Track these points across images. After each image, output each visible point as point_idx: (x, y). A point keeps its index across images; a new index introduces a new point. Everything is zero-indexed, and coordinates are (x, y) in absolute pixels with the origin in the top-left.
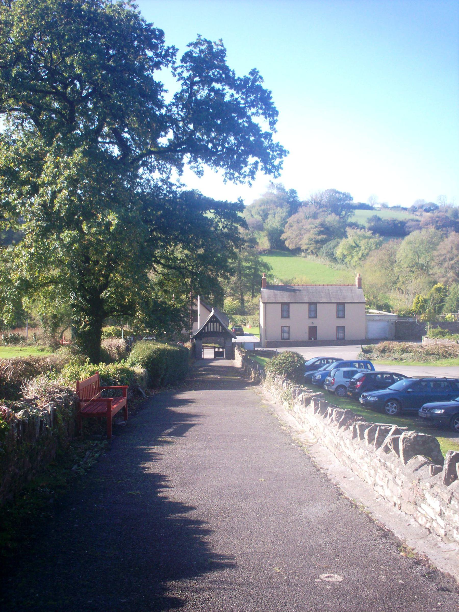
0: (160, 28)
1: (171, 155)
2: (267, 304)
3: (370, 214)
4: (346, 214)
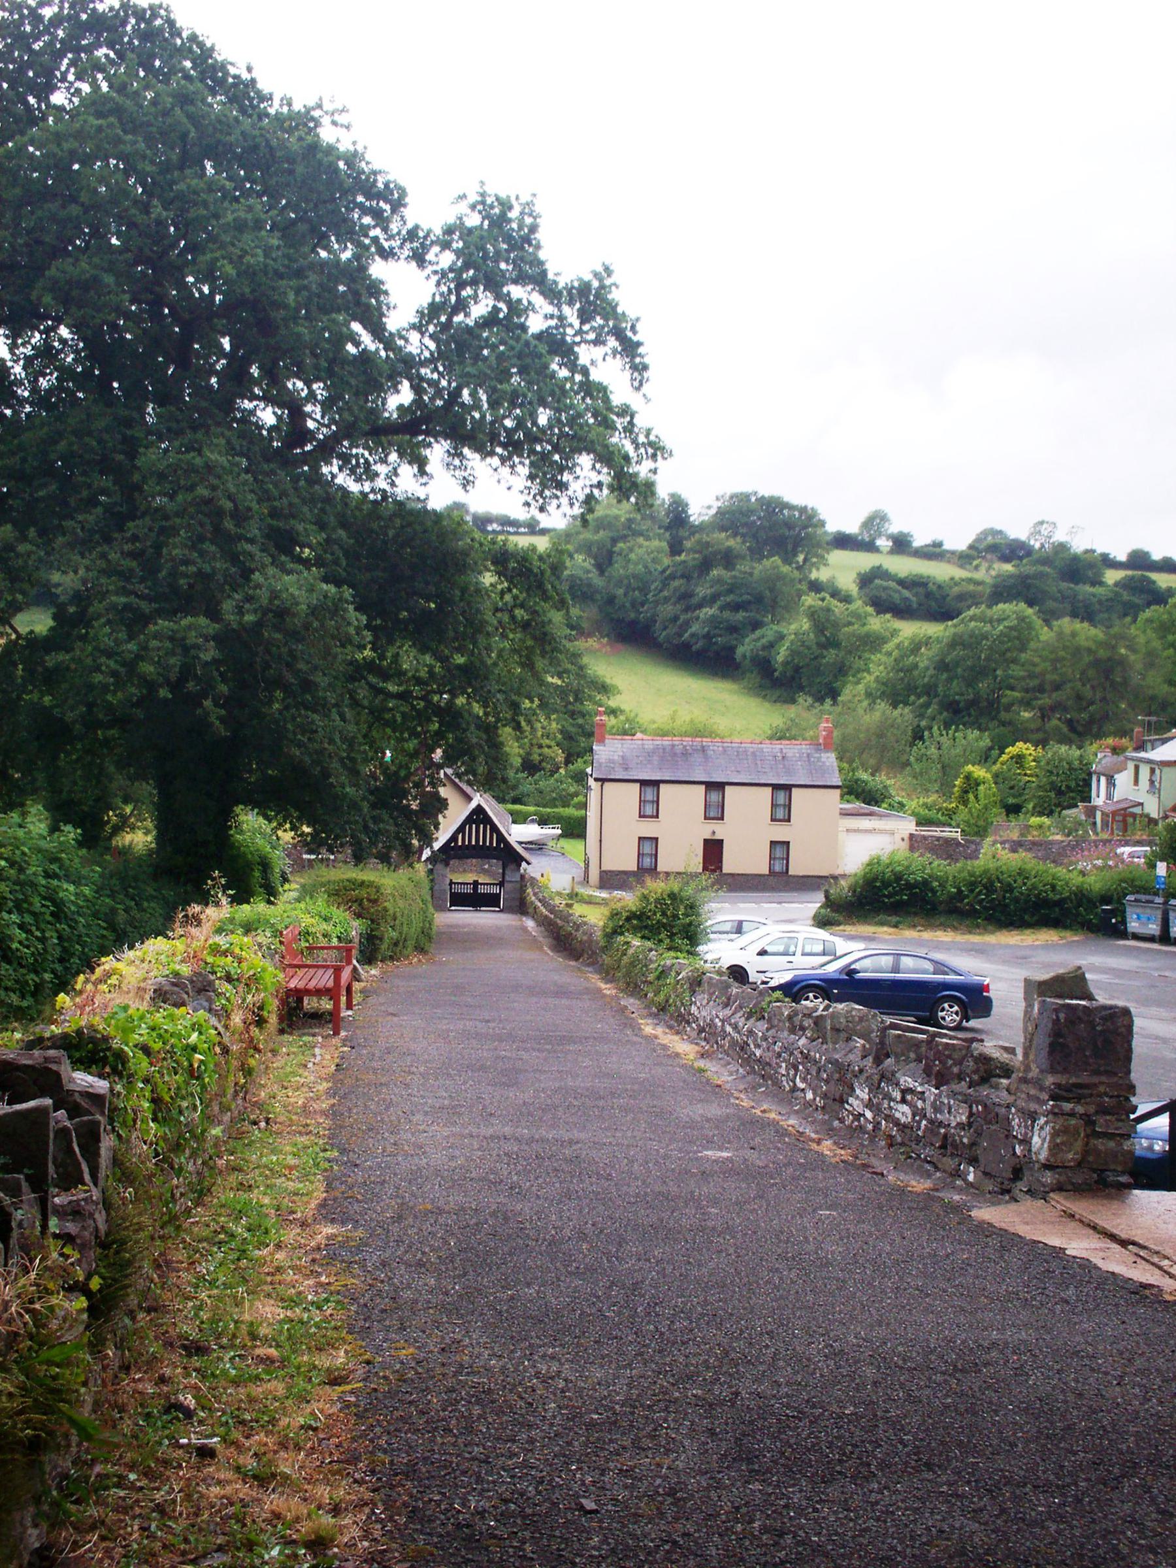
0: (402, 183)
1: (408, 434)
2: (607, 785)
3: (865, 561)
4: (805, 560)
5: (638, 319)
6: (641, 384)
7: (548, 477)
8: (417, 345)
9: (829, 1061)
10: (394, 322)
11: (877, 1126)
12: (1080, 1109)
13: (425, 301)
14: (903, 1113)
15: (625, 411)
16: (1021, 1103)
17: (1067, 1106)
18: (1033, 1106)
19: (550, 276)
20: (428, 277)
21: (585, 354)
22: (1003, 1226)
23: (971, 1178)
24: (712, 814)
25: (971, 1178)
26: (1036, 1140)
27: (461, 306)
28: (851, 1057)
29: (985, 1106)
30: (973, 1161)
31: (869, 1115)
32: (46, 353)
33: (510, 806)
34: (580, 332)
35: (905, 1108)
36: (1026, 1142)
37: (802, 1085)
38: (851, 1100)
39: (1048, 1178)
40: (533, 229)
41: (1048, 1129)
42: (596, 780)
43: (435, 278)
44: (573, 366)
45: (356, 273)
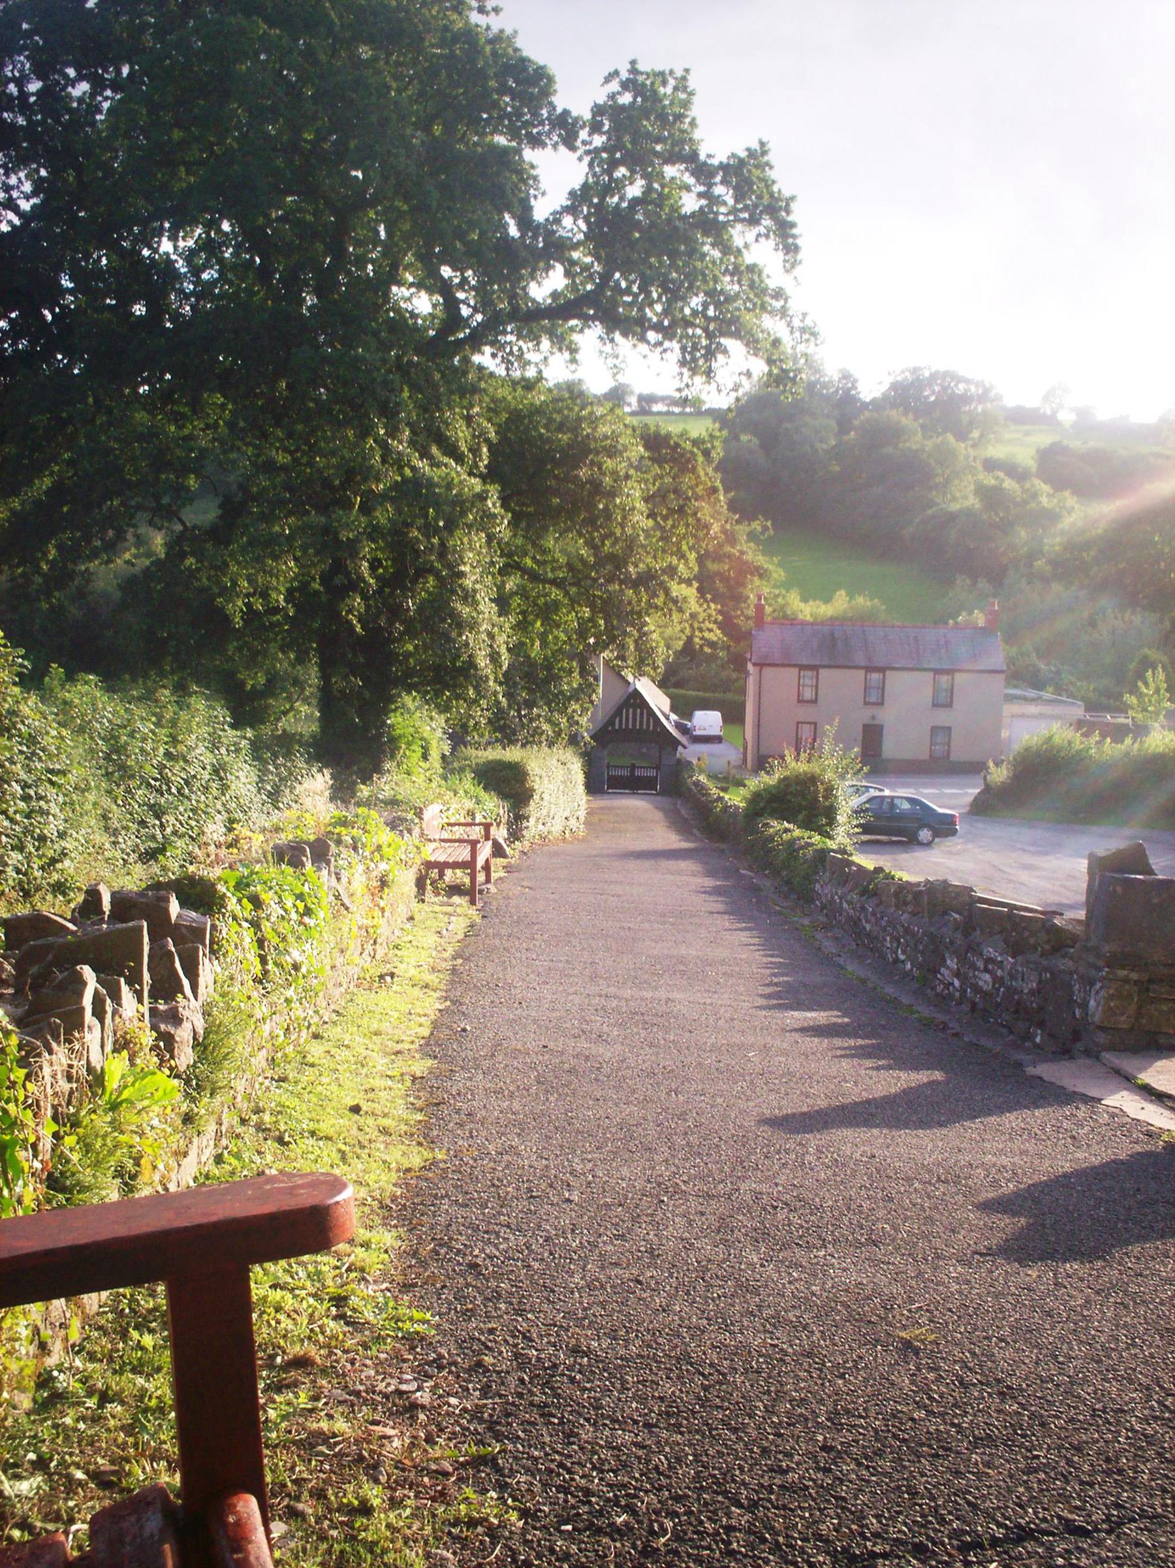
2: (767, 671)
4: (982, 436)
5: (793, 198)
6: (793, 267)
7: (699, 360)
8: (573, 227)
9: (924, 934)
10: (541, 211)
11: (963, 991)
12: (1134, 976)
13: (576, 182)
14: (985, 980)
15: (778, 294)
16: (1081, 970)
17: (1122, 973)
18: (1093, 972)
19: (702, 157)
20: (580, 159)
21: (739, 235)
22: (1053, 1080)
23: (1038, 1040)
24: (873, 699)
25: (1038, 1040)
26: (1092, 1003)
27: (616, 186)
28: (944, 930)
29: (1052, 974)
30: (1041, 1024)
31: (957, 983)
32: (209, 247)
33: (672, 690)
34: (734, 211)
35: (987, 977)
36: (1084, 1005)
37: (902, 957)
38: (943, 970)
39: (1101, 1038)
40: (686, 104)
41: (1102, 993)
42: (754, 664)
43: (587, 159)
44: (727, 248)
45: (507, 161)
